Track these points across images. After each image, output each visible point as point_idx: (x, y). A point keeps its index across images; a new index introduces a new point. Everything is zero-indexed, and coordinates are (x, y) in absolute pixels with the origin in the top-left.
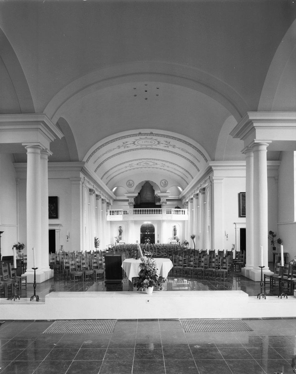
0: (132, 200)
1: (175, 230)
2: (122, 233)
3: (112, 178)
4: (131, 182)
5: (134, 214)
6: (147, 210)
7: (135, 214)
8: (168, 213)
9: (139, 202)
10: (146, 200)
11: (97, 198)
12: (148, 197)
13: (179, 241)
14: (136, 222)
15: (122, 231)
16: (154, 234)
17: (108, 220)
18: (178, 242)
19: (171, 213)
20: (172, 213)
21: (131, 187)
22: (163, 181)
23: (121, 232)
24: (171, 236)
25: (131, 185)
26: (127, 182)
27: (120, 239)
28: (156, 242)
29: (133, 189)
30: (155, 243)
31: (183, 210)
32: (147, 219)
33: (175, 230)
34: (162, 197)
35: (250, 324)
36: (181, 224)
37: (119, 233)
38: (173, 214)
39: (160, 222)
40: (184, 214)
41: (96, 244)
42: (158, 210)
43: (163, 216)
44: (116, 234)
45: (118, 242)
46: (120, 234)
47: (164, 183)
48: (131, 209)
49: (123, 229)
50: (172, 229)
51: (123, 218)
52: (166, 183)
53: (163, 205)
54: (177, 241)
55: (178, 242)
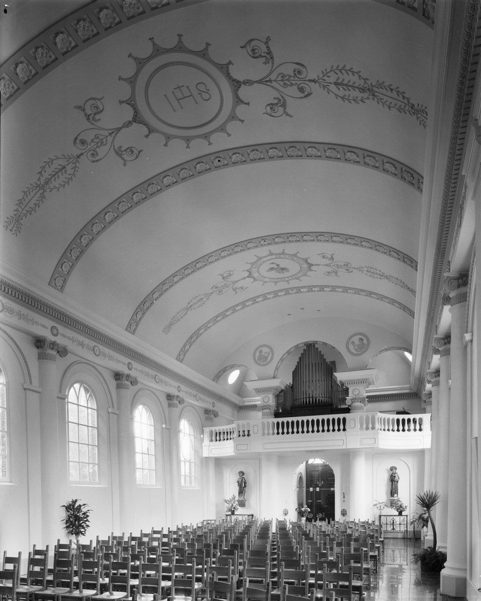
0: (271, 401)
1: (393, 480)
2: (246, 489)
3: (197, 334)
4: (265, 350)
5: (273, 434)
6: (308, 421)
7: (278, 433)
8: (241, 433)
9: (289, 404)
10: (313, 396)
11: (39, 354)
12: (316, 391)
13: (403, 513)
14: (283, 460)
15: (245, 483)
16: (334, 491)
17: (205, 454)
18: (400, 514)
19: (373, 428)
20: (377, 426)
21: (264, 365)
22: (356, 339)
23: (243, 486)
24: (383, 495)
25: (266, 358)
26: (256, 350)
27: (242, 504)
28: (338, 516)
29: (270, 369)
30: (333, 519)
31: (417, 416)
32: (314, 447)
33: (393, 480)
34: (353, 382)
35: (299, 346)
36: (412, 462)
37: (237, 488)
38: (380, 431)
39: (347, 457)
40: (420, 430)
41: (76, 520)
42: (334, 420)
43: (352, 438)
44: (232, 490)
45: (233, 513)
46: (241, 492)
47: (357, 342)
48: (260, 421)
49: (250, 478)
50: (386, 476)
51: (236, 447)
52: (365, 342)
53: (356, 408)
54: (397, 513)
55: (400, 514)
